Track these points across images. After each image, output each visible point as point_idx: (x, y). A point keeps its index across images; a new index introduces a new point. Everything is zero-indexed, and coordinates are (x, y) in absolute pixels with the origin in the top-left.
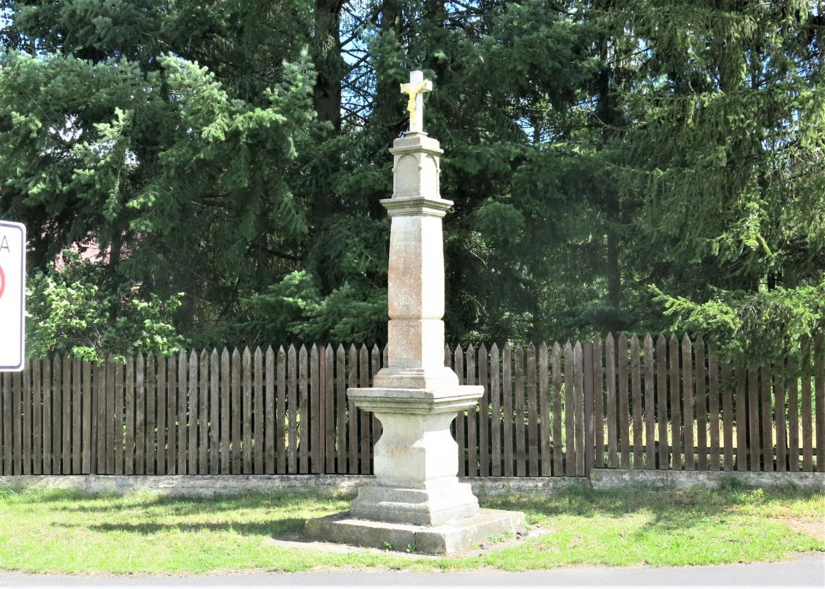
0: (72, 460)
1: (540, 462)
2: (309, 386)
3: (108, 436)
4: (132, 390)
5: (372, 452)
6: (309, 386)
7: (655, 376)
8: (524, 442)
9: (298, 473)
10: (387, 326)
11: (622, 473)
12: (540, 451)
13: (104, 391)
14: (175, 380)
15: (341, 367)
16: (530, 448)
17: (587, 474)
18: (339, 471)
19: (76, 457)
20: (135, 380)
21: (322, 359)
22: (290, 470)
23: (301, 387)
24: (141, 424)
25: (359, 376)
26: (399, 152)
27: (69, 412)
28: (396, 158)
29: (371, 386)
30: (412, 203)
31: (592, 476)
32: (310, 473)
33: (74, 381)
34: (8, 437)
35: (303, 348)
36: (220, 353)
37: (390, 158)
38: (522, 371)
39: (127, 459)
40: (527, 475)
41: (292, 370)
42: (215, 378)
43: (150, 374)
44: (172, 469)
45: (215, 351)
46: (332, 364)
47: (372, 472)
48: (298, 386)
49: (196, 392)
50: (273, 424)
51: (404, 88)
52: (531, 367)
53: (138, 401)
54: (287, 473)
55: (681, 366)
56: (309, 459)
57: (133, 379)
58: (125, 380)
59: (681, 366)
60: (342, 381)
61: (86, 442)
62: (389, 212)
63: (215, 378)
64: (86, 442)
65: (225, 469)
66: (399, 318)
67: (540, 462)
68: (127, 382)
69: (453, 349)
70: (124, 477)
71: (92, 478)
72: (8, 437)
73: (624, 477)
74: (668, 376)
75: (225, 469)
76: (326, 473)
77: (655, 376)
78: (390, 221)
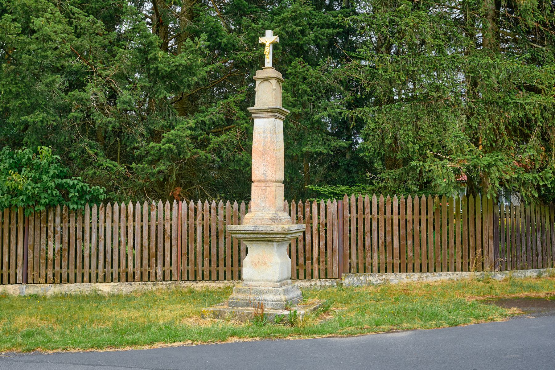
0: (9, 274)
1: (312, 270)
2: (171, 225)
3: (35, 259)
4: (52, 229)
5: (240, 265)
6: (171, 225)
7: (378, 219)
8: (303, 259)
9: (164, 280)
10: (251, 187)
11: (360, 276)
12: (312, 264)
13: (32, 229)
14: (82, 222)
15: (192, 214)
16: (307, 262)
17: (340, 277)
18: (11, 282)
19: (12, 272)
20: (54, 222)
21: (180, 209)
22: (159, 279)
23: (166, 226)
24: (58, 251)
25: (203, 219)
26: (259, 79)
27: (7, 242)
28: (257, 83)
29: (239, 224)
30: (269, 110)
31: (343, 278)
32: (171, 280)
33: (12, 222)
34: (465, 245)
35: (168, 202)
36: (126, 205)
37: (254, 81)
38: (302, 216)
39: (49, 273)
40: (305, 278)
41: (160, 215)
42: (109, 220)
43: (65, 218)
44: (308, 276)
45: (109, 204)
46: (186, 212)
47: (240, 278)
48: (164, 225)
49: (96, 230)
50: (147, 250)
51: (262, 40)
52: (308, 214)
53: (56, 236)
54: (157, 280)
55: (392, 214)
56: (171, 271)
57: (53, 222)
58: (47, 222)
59: (392, 214)
60: (192, 223)
61: (20, 262)
62: (253, 115)
63: (109, 220)
64: (20, 262)
65: (115, 279)
66: (259, 181)
67: (312, 270)
68: (49, 224)
69: (290, 202)
70: (46, 285)
71: (24, 286)
72: (465, 245)
73: (361, 278)
74: (385, 219)
75: (115, 279)
76: (181, 280)
77: (378, 219)
78: (253, 122)
